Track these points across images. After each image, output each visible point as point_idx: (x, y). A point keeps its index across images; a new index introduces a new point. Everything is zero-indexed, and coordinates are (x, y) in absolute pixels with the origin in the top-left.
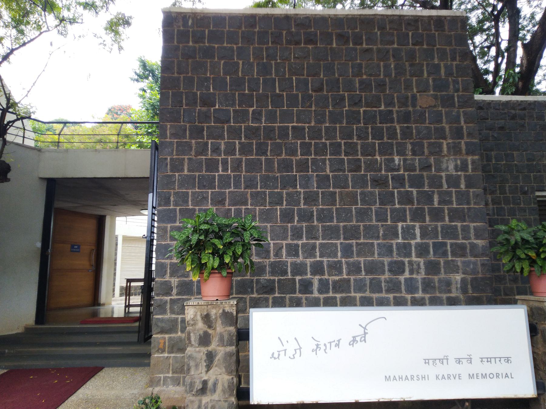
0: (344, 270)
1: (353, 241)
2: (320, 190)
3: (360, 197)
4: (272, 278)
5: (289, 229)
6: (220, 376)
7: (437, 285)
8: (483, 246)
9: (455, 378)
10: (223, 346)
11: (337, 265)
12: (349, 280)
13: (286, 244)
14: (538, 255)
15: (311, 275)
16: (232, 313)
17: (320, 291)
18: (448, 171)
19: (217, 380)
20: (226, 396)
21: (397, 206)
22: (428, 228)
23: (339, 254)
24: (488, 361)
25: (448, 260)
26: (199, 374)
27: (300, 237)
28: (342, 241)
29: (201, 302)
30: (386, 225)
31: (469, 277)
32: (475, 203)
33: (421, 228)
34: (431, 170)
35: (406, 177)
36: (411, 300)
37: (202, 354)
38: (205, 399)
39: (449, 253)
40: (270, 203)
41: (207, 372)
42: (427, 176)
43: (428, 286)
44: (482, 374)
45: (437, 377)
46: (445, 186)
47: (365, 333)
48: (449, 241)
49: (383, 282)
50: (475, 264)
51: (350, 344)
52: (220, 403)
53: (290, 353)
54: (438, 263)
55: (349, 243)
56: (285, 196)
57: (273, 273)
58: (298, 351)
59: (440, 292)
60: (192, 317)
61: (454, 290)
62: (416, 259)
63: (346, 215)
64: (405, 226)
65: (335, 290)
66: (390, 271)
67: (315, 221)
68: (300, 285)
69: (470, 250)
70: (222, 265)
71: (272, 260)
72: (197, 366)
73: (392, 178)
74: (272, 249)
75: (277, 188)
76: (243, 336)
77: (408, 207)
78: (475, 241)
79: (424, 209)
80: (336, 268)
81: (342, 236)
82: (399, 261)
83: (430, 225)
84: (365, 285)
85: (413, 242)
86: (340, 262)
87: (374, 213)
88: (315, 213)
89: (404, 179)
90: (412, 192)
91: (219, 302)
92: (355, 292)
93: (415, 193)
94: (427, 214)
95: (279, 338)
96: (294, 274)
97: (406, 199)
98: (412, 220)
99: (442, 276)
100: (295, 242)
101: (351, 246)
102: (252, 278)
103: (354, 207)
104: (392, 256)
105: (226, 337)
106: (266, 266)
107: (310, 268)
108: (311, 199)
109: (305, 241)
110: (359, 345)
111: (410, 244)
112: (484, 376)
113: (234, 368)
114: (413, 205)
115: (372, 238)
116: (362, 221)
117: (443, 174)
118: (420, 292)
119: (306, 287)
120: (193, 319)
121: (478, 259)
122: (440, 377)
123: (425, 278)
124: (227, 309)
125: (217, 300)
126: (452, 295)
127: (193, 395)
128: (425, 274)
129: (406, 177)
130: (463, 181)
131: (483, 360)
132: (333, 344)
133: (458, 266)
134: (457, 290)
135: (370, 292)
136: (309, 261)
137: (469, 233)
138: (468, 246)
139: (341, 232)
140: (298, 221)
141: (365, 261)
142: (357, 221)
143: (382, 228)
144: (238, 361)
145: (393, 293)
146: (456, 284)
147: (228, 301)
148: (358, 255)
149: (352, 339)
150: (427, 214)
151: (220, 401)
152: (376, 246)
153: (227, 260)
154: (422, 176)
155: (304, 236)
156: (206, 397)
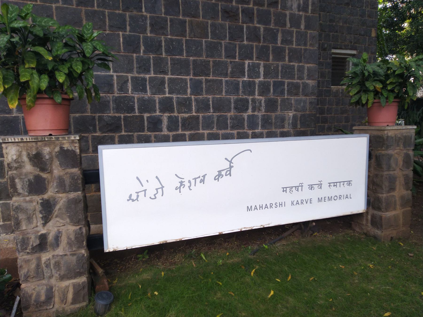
0: (194, 108)
1: (203, 77)
2: (169, 17)
3: (211, 30)
4: (117, 115)
5: (135, 61)
6: (64, 227)
7: (273, 121)
8: (313, 85)
9: (307, 203)
10: (65, 192)
11: (186, 102)
12: (198, 117)
13: (132, 78)
14: (385, 87)
15: (160, 112)
16: (74, 152)
17: (170, 129)
18: (292, 10)
19: (59, 232)
20: (74, 249)
21: (245, 42)
22: (270, 67)
23: (189, 91)
24: (334, 186)
25: (284, 99)
26: (35, 228)
27: (148, 71)
28: (191, 77)
29: (26, 138)
30: (234, 62)
31: (299, 114)
32: (311, 45)
33: (265, 66)
34: (277, 7)
35: (255, 12)
36: (252, 135)
37: (35, 204)
38: (45, 257)
39: (286, 92)
40: (111, 26)
41: (44, 224)
42: (274, 13)
43: (266, 122)
44: (329, 197)
45: (292, 203)
46: (288, 25)
47: (231, 167)
48: (286, 81)
49: (229, 119)
50: (305, 102)
51: (215, 179)
52: (66, 257)
53: (151, 193)
54: (276, 101)
55: (198, 80)
56: (128, 19)
57: (118, 109)
58: (160, 191)
59: (276, 128)
60: (15, 157)
61: (286, 126)
62: (258, 97)
63: (196, 48)
64: (251, 64)
65: (185, 128)
66: (235, 108)
67: (164, 53)
68: (149, 122)
69: (303, 90)
70: (54, 87)
71: (116, 95)
72: (29, 219)
73: (243, 11)
74: (115, 82)
75: (118, 8)
76: (91, 178)
77: (255, 44)
78: (307, 81)
79: (269, 47)
80: (185, 105)
81: (192, 72)
82: (243, 99)
83: (273, 64)
84: (213, 122)
85: (257, 81)
86: (190, 99)
87: (223, 49)
88: (163, 44)
89: (253, 14)
90: (259, 28)
91: (53, 137)
92: (203, 129)
93: (262, 30)
94: (271, 52)
95: (137, 178)
96: (141, 111)
97: (254, 35)
98: (258, 58)
99: (279, 113)
100: (142, 76)
101: (200, 82)
102: (94, 115)
103: (204, 40)
104: (238, 94)
105: (68, 181)
106: (109, 102)
107: (159, 105)
108: (158, 26)
109: (152, 75)
110: (225, 179)
111: (254, 82)
112: (330, 199)
113: (81, 216)
114: (259, 42)
115: (221, 75)
116: (212, 57)
117: (288, 13)
118: (260, 128)
119: (155, 124)
120: (16, 161)
121: (308, 97)
122: (295, 203)
123: (264, 115)
124: (66, 146)
125: (51, 135)
126: (285, 130)
127: (28, 253)
128: (265, 112)
129: (255, 12)
130: (303, 22)
131: (331, 184)
132: (198, 180)
133: (292, 104)
134: (289, 125)
135: (217, 129)
136: (157, 97)
137: (303, 73)
138: (301, 85)
139: (191, 67)
140: (144, 51)
141: (213, 98)
142: (207, 56)
143: (230, 65)
144: (86, 208)
145: (237, 129)
146: (289, 120)
147: (66, 137)
148: (207, 93)
149: (218, 173)
150: (271, 52)
151: (66, 255)
152: (224, 83)
153: (61, 79)
154: (269, 13)
155: (152, 69)
156: (47, 254)
